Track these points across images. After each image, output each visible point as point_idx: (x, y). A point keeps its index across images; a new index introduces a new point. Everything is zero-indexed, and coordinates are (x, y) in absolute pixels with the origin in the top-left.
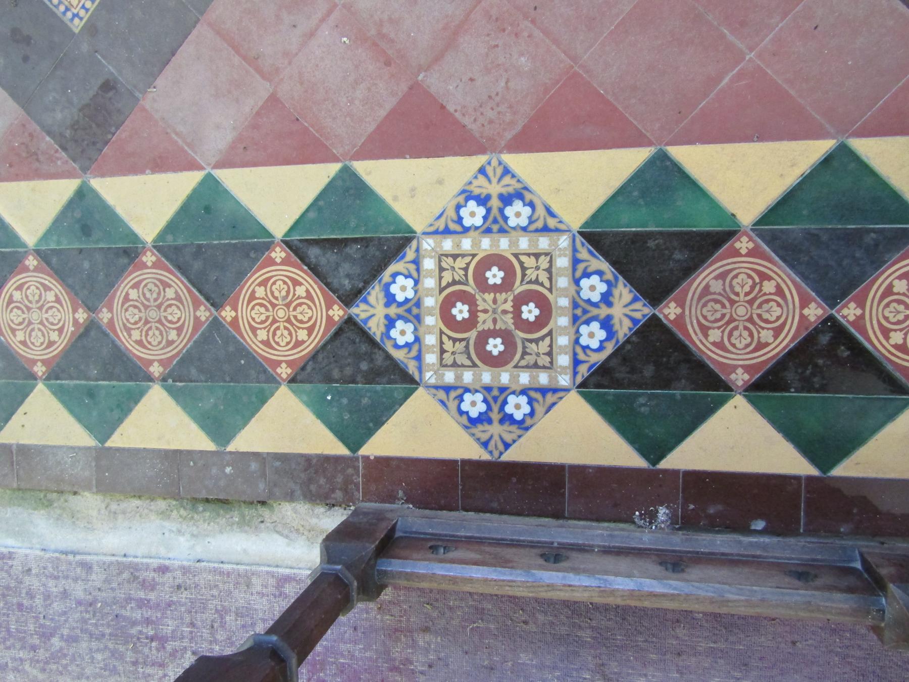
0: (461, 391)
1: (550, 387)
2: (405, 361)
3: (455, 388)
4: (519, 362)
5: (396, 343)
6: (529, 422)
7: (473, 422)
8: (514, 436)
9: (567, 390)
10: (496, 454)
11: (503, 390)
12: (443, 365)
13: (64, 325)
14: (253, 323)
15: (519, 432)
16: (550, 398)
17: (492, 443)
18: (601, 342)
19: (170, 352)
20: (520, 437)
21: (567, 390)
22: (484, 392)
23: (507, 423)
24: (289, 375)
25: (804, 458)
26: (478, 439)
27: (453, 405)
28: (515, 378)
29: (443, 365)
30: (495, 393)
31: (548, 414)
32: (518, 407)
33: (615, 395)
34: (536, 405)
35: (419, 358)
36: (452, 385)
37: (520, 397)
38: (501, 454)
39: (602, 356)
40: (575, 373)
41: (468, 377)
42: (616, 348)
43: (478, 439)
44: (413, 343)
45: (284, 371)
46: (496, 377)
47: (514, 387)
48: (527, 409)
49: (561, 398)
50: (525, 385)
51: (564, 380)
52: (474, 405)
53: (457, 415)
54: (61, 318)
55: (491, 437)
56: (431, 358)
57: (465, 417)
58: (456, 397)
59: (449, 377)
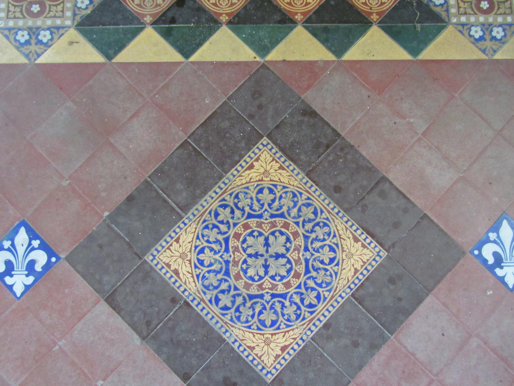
0: (15, 30)
1: (61, 26)
2: (440, 12)
3: (467, 25)
4: (496, 12)
5: (435, 4)
6: (50, 43)
7: (477, 40)
8: (42, 51)
9: (69, 27)
10: (33, 60)
11: (490, 25)
12: (63, 17)
13: (218, 7)
14: (154, 5)
15: (500, 45)
16: (61, 31)
17: (31, 55)
18: (87, 5)
19: (159, 10)
20: (45, 51)
21: (69, 27)
22: (28, 30)
23: (494, 40)
24: (151, 21)
26: (24, 53)
27: (12, 38)
28: (495, 20)
29: (63, 17)
30: (486, 26)
31: (59, 40)
32: (498, 32)
33: (113, 28)
34: (54, 35)
35: (447, 11)
36: (465, 23)
37: (477, 27)
38: (35, 60)
39: (89, 12)
40: (74, 20)
41: (472, 19)
42: (94, 8)
43: (24, 53)
44: (444, 4)
45: (224, 19)
46: (486, 19)
47: (495, 24)
48: (502, 34)
49: (66, 31)
50: (49, 25)
51: (68, 23)
52: (23, 37)
53: (13, 42)
54: (297, 5)
55: (487, 47)
56: (453, 11)
57: (472, 38)
58: (467, 29)
59: (463, 19)
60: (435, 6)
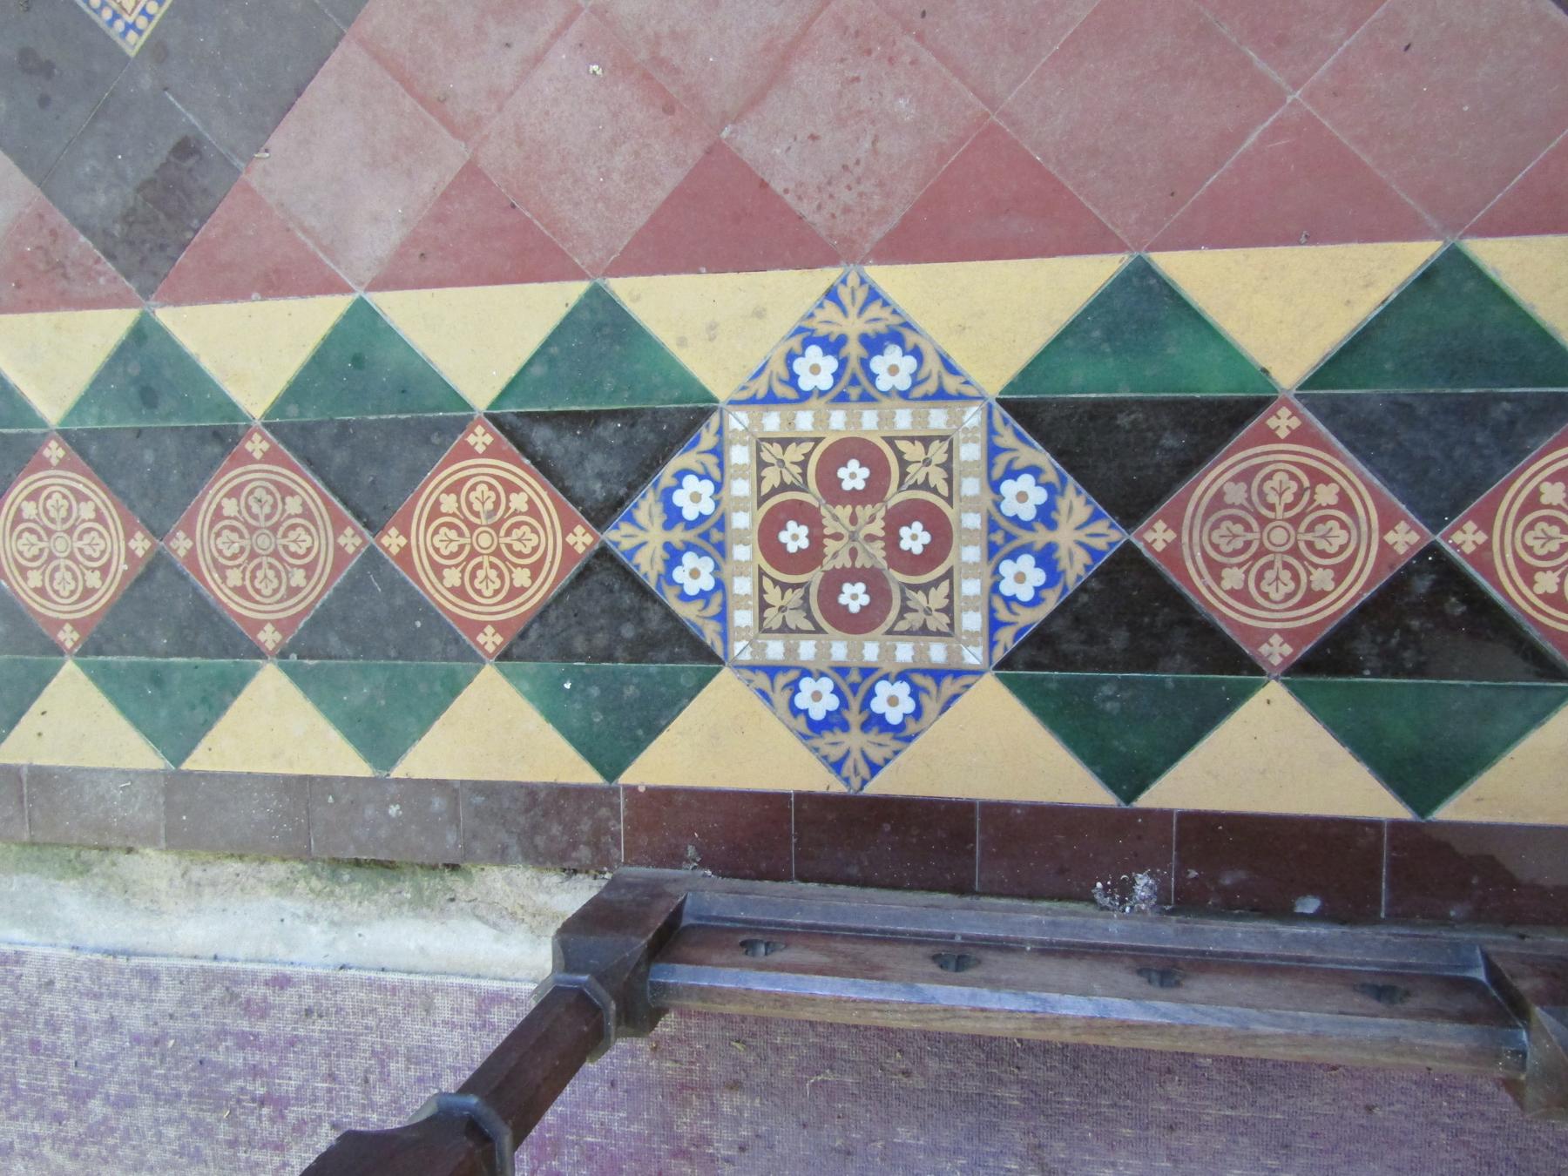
0: (795, 674)
1: (949, 668)
2: (699, 622)
3: (785, 669)
4: (894, 624)
5: (683, 591)
6: (912, 727)
7: (817, 727)
8: (887, 752)
9: (978, 673)
10: (856, 782)
11: (867, 672)
12: (764, 630)
15: (896, 745)
16: (949, 686)
17: (849, 764)
18: (1037, 589)
19: (294, 607)
20: (896, 753)
21: (978, 673)
22: (836, 676)
23: (875, 729)
24: (498, 647)
25: (1387, 789)
26: (825, 757)
27: (781, 698)
28: (888, 652)
29: (764, 630)
30: (854, 677)
31: (946, 714)
32: (893, 701)
33: (1060, 681)
34: (924, 698)
35: (722, 617)
36: (780, 664)
37: (898, 684)
38: (864, 782)
39: (1039, 615)
40: (992, 644)
41: (807, 650)
42: (1062, 600)
43: (825, 757)
44: (713, 592)
45: (490, 640)
46: (855, 651)
47: (886, 667)
48: (908, 706)
49: (968, 687)
50: (906, 664)
51: (973, 656)
52: (818, 698)
53: (788, 716)
55: (848, 753)
56: (743, 618)
57: (802, 719)
58: (787, 685)
60: (684, 597)
